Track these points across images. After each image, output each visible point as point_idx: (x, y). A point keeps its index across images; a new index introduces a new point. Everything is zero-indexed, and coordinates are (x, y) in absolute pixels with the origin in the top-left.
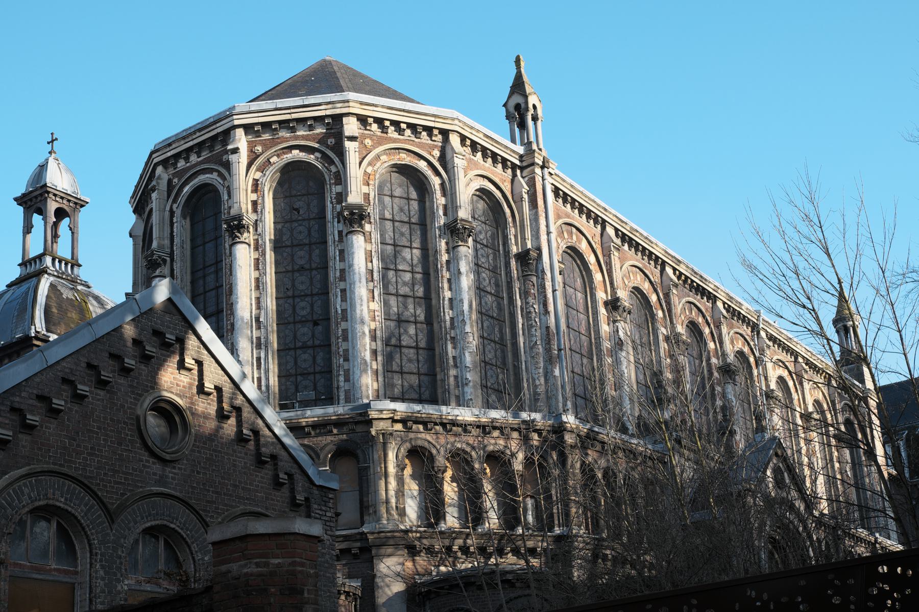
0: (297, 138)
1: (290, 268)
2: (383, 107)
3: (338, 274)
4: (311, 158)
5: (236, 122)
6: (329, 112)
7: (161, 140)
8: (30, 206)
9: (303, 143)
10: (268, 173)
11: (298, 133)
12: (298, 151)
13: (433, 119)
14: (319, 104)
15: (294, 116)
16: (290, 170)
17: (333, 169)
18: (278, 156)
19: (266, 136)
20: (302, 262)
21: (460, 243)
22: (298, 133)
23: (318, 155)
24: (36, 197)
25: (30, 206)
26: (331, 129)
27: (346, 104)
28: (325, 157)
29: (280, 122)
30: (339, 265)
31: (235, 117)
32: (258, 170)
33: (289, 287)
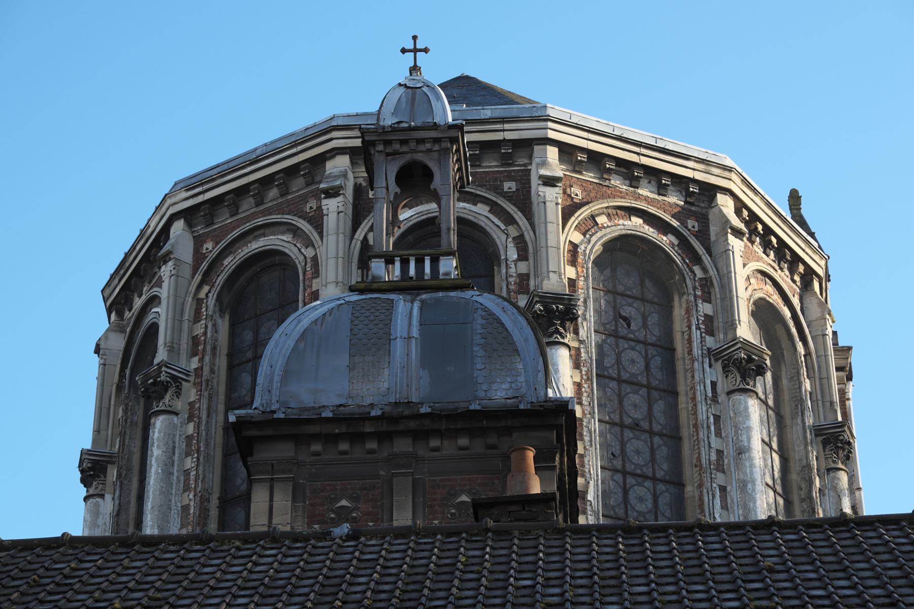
0: (639, 197)
1: (616, 418)
2: (763, 198)
3: (714, 457)
4: (665, 241)
5: (552, 135)
6: (699, 176)
7: (353, 111)
8: (395, 153)
9: (652, 210)
10: (594, 239)
11: (640, 191)
12: (640, 221)
13: (803, 245)
14: (687, 157)
15: (645, 161)
16: (621, 249)
17: (699, 274)
18: (609, 216)
19: (589, 176)
20: (637, 415)
21: (840, 466)
22: (640, 191)
23: (672, 238)
24: (420, 141)
25: (395, 153)
26: (692, 204)
27: (726, 174)
28: (684, 244)
29: (620, 162)
30: (715, 443)
31: (550, 124)
32: (577, 228)
33: (617, 453)
